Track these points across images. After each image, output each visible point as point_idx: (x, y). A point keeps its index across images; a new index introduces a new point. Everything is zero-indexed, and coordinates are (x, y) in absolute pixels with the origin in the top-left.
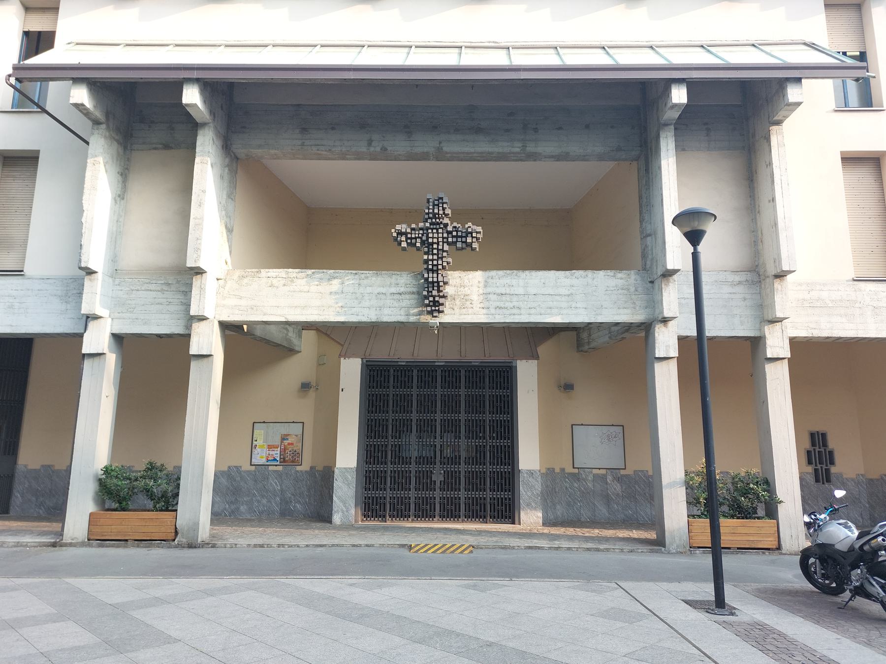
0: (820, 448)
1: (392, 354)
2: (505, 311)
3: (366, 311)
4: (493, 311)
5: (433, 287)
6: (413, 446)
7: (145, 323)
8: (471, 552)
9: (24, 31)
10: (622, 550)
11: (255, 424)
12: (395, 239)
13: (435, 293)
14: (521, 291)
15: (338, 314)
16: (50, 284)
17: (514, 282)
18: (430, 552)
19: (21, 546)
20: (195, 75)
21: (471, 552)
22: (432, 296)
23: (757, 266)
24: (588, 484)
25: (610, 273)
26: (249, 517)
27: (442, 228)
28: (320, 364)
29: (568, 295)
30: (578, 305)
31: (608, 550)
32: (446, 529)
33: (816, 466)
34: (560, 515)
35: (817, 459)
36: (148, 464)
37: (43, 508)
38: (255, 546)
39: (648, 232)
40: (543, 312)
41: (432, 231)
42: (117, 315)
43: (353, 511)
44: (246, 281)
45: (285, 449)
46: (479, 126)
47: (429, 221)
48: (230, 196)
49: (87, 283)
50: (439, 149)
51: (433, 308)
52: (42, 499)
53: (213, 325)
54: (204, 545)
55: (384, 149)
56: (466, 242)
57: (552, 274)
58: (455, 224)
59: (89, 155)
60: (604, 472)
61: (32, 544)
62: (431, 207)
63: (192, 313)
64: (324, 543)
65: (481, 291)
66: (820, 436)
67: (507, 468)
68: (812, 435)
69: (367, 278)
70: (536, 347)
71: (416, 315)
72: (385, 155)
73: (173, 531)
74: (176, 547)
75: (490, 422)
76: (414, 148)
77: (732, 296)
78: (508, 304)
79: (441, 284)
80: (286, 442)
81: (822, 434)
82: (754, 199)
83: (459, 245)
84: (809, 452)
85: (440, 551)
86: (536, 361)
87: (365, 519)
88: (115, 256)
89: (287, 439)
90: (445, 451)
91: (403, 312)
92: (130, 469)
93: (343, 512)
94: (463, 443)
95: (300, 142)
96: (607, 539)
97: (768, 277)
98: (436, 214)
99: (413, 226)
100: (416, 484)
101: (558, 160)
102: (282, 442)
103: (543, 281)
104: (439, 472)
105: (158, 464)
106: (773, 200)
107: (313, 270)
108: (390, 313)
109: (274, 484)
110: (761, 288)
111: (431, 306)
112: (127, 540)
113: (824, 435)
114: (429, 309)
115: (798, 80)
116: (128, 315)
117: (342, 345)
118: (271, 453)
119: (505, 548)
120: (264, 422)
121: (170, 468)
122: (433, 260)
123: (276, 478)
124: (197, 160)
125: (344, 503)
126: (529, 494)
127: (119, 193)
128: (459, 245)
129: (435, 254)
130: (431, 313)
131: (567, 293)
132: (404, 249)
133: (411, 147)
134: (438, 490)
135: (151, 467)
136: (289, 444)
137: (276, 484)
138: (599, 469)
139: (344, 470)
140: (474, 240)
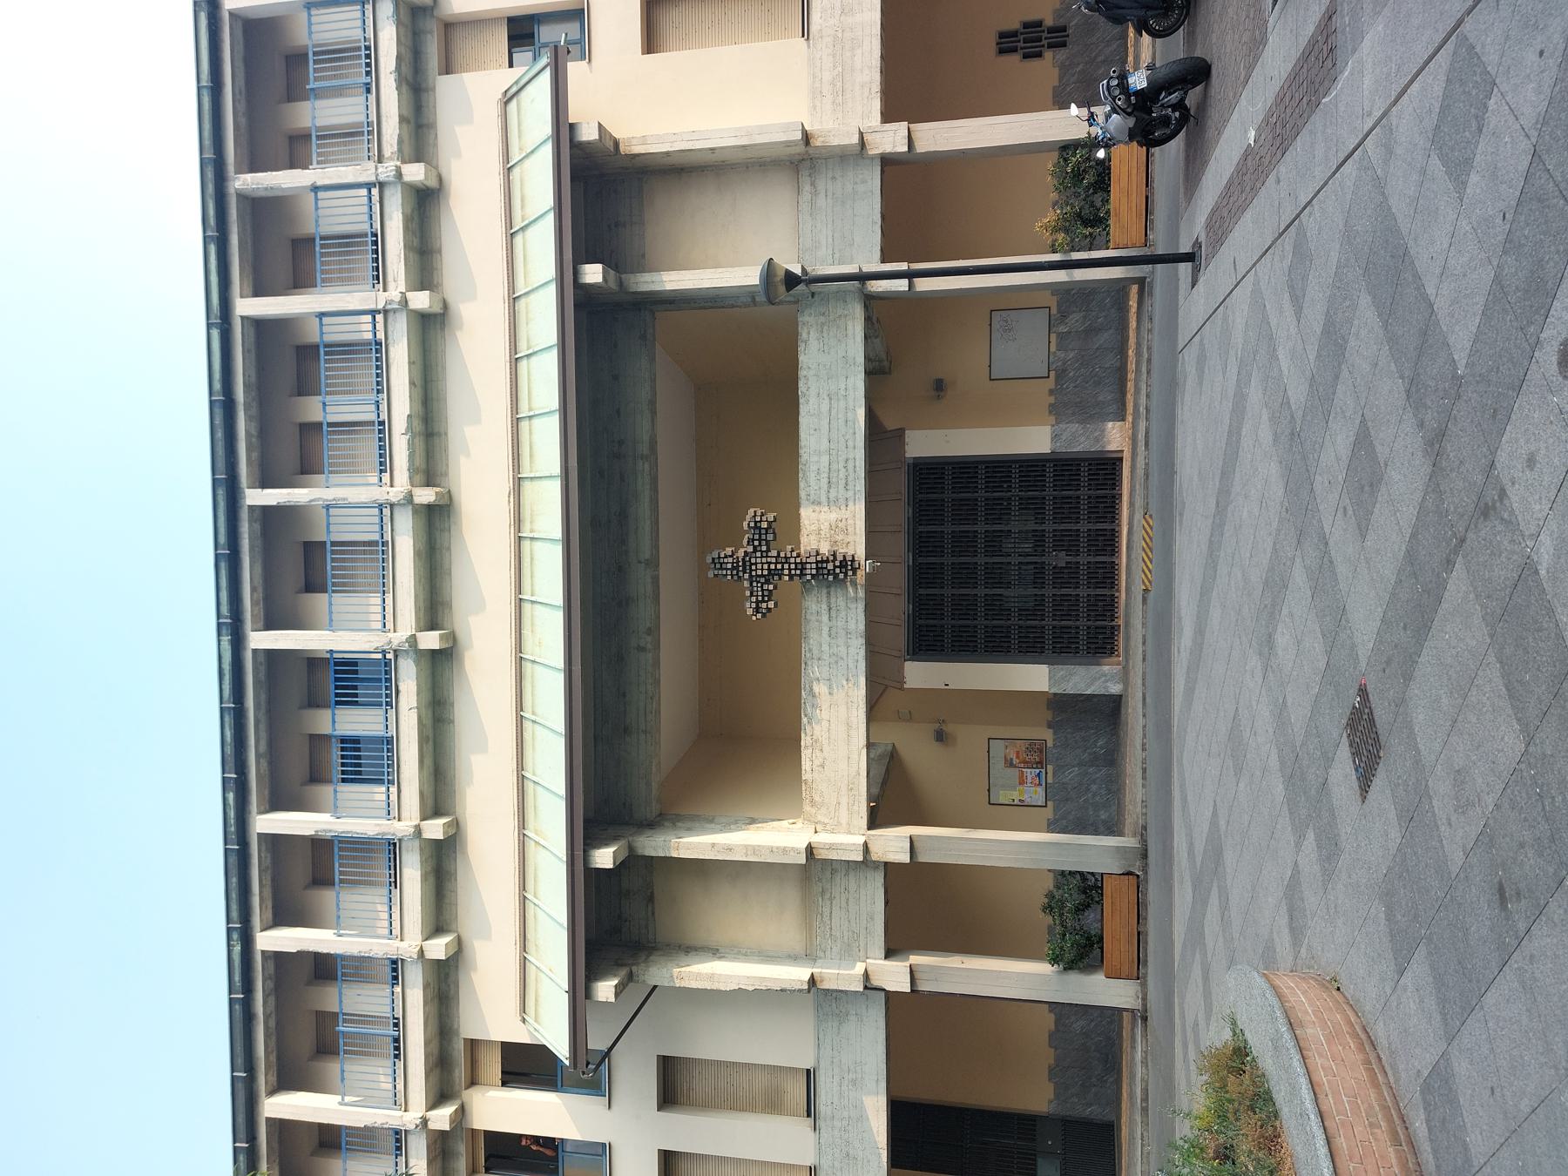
0: (1019, 41)
1: (898, 622)
2: (850, 479)
3: (852, 651)
4: (850, 493)
5: (822, 568)
6: (1016, 594)
7: (872, 919)
8: (1151, 516)
9: (502, 1086)
10: (1150, 331)
11: (992, 802)
12: (764, 615)
13: (830, 566)
14: (825, 459)
15: (856, 684)
16: (825, 1035)
17: (814, 468)
18: (1151, 567)
19: (1146, 1058)
20: (579, 853)
21: (1151, 516)
22: (834, 570)
23: (791, 163)
24: (1071, 357)
25: (801, 348)
26: (1115, 808)
27: (750, 559)
28: (910, 718)
29: (830, 399)
30: (843, 387)
31: (1149, 348)
32: (1128, 548)
33: (1043, 46)
34: (1113, 395)
35: (1033, 30)
36: (1045, 912)
37: (1105, 1078)
38: (1144, 778)
39: (750, 300)
40: (851, 431)
41: (753, 564)
42: (862, 953)
43: (1106, 668)
44: (817, 798)
45: (1025, 762)
46: (617, 514)
47: (741, 574)
48: (712, 821)
49: (826, 986)
50: (647, 563)
51: (849, 568)
52: (1094, 1079)
53: (873, 835)
54: (1144, 842)
55: (649, 631)
56: (766, 529)
57: (804, 421)
58: (745, 541)
59: (672, 984)
60: (1053, 337)
61: (1144, 1046)
62: (724, 572)
63: (860, 858)
64: (1141, 695)
65: (826, 509)
66: (1003, 40)
67: (1049, 469)
68: (1002, 51)
69: (810, 650)
70: (886, 432)
71: (857, 589)
72: (654, 631)
73: (1126, 877)
74: (1146, 873)
75: (988, 492)
76: (648, 594)
77: (830, 194)
78: (842, 474)
79: (819, 558)
80: (1015, 761)
81: (1000, 38)
82: (705, 167)
83: (770, 537)
84: (1026, 56)
85: (1150, 554)
86: (907, 432)
87: (1116, 653)
88: (789, 957)
89: (1012, 759)
90: (1027, 550)
91: (853, 606)
92: (1050, 930)
93: (1107, 681)
94: (1015, 526)
95: (642, 737)
96: (1138, 345)
97: (807, 151)
98: (732, 565)
99: (748, 593)
100: (1070, 588)
101: (655, 413)
102: (1015, 767)
103: (812, 432)
104: (1054, 558)
105: (1046, 900)
106: (712, 149)
107: (803, 716)
108: (854, 621)
109: (1071, 775)
110: (819, 158)
111: (847, 570)
112: (1139, 933)
113: (1002, 35)
114: (850, 573)
115: (572, 127)
117: (887, 687)
118: (1029, 780)
119: (1147, 475)
120: (989, 790)
121: (1049, 884)
122: (790, 569)
123: (1064, 772)
124: (675, 855)
125: (1095, 679)
126: (1083, 439)
127: (711, 955)
128: (770, 537)
129: (783, 566)
130: (854, 570)
131: (827, 401)
132: (776, 605)
133: (645, 599)
134: (1078, 559)
135: (1048, 908)
136: (1018, 757)
137: (1070, 773)
138: (1049, 342)
139: (1052, 681)
140: (764, 518)
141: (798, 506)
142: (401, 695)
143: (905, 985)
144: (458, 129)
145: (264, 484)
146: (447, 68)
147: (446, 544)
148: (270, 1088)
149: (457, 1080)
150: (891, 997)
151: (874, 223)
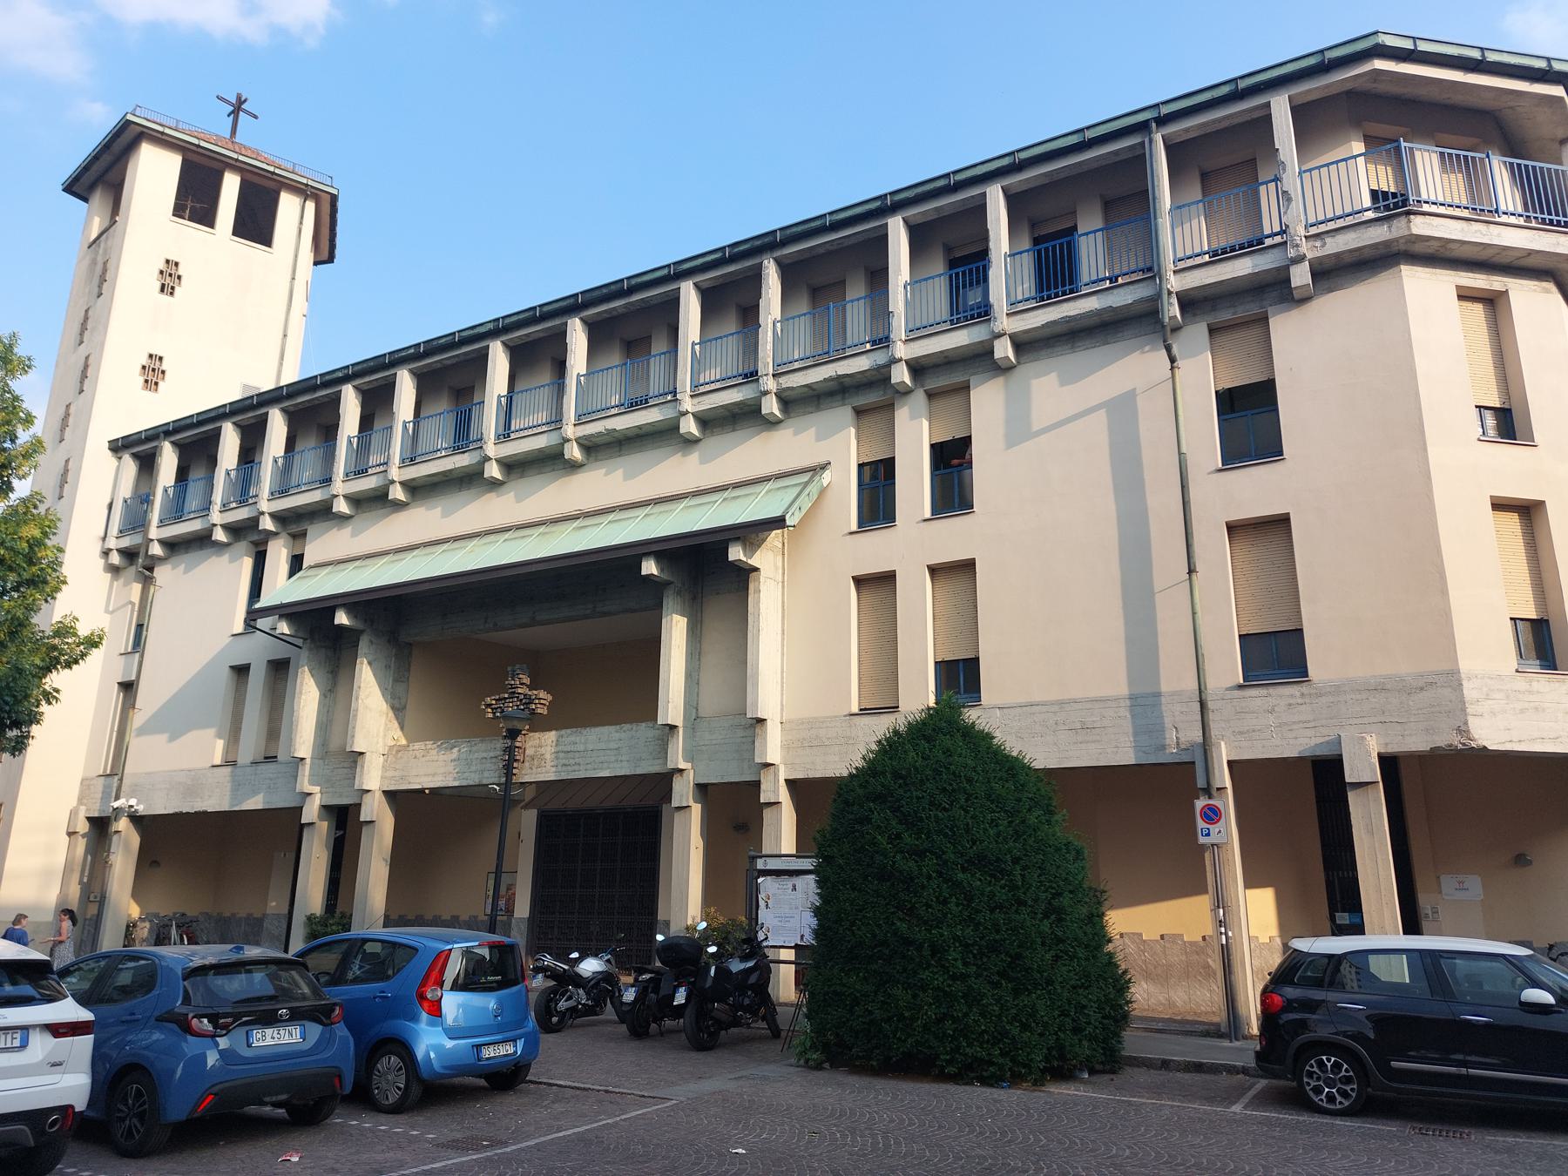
2: (569, 768)
3: (473, 775)
14: (581, 748)
15: (455, 779)
30: (624, 758)
65: (553, 751)
69: (476, 744)
77: (744, 740)
116: (331, 789)
131: (616, 746)
141: (556, 729)
142: (462, 455)
143: (366, 816)
144: (1053, 375)
145: (1296, 110)
146: (859, 412)
147: (556, 467)
148: (239, 423)
149: (291, 527)
150: (298, 811)
151: (722, 777)
